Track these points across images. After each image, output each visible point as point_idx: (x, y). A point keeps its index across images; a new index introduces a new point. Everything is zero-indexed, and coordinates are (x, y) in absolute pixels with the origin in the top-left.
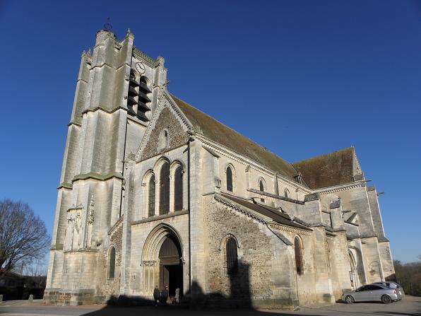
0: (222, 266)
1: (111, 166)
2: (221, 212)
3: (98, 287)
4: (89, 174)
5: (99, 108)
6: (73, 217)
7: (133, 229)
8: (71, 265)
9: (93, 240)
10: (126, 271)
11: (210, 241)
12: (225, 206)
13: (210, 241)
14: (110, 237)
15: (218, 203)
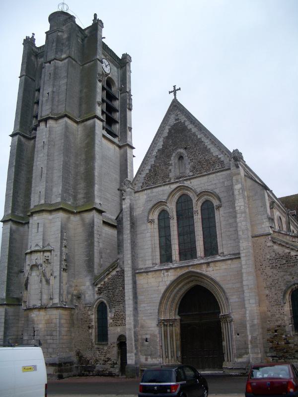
0: (287, 322)
1: (86, 193)
2: (282, 257)
3: (78, 354)
4: (59, 203)
5: (66, 116)
6: (40, 261)
7: (142, 280)
8: (41, 326)
9: (68, 293)
10: (135, 333)
11: (267, 292)
12: (287, 251)
13: (267, 292)
14: (97, 289)
15: (276, 247)
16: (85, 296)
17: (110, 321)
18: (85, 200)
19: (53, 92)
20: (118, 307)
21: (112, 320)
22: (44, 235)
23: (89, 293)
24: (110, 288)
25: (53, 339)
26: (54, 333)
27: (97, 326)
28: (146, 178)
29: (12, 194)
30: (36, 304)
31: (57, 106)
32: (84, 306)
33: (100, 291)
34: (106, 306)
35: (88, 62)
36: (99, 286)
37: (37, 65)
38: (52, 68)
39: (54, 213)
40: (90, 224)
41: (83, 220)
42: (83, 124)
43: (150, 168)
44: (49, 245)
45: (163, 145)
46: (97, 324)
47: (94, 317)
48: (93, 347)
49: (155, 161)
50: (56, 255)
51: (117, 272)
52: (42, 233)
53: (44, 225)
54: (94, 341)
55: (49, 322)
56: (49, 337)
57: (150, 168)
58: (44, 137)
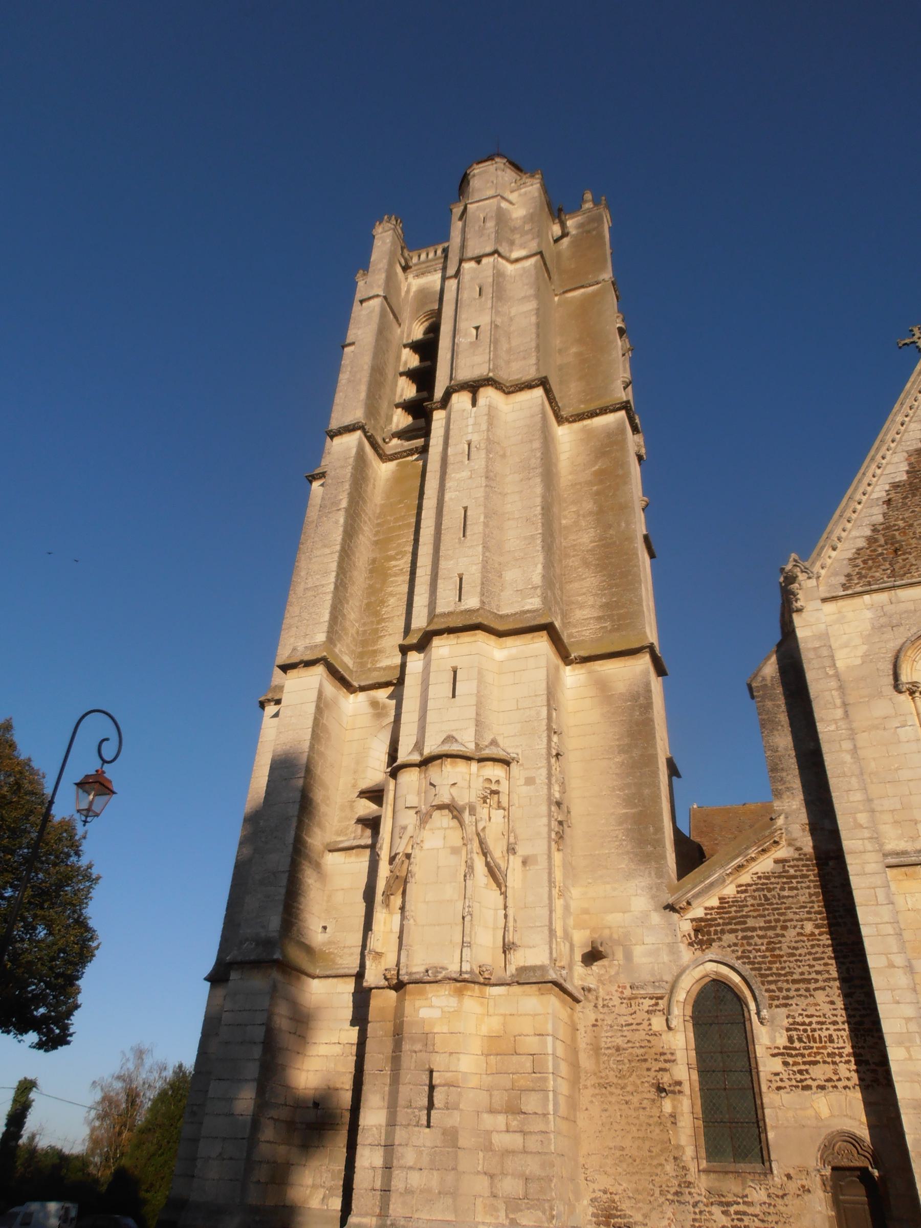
14: (686, 927)
16: (628, 956)
17: (768, 1066)
18: (607, 624)
19: (495, 326)
20: (803, 1003)
21: (779, 1060)
22: (479, 705)
23: (647, 940)
24: (751, 923)
25: (524, 1133)
26: (531, 1103)
27: (697, 1086)
28: (859, 561)
29: (332, 587)
30: (445, 962)
31: (508, 362)
32: (628, 992)
33: (703, 934)
34: (740, 1001)
35: (582, 287)
36: (698, 912)
37: (408, 292)
38: (490, 272)
39: (509, 641)
40: (634, 697)
41: (602, 686)
42: (577, 426)
43: (868, 532)
44: (494, 743)
45: (908, 472)
46: (695, 1076)
47: (680, 1041)
48: (689, 1184)
49: (884, 515)
50: (530, 781)
51: (777, 862)
52: (473, 701)
53: (480, 673)
54: (689, 1152)
55: (501, 1047)
56: (501, 1119)
57: (868, 532)
58: (470, 429)
